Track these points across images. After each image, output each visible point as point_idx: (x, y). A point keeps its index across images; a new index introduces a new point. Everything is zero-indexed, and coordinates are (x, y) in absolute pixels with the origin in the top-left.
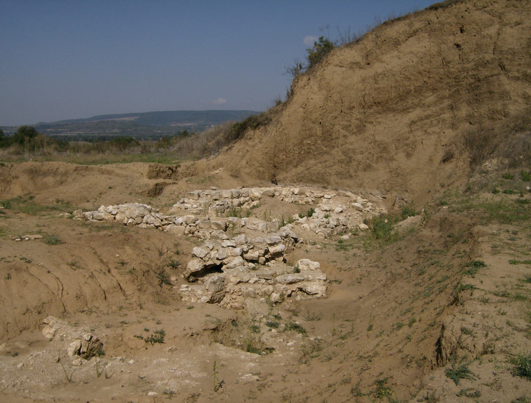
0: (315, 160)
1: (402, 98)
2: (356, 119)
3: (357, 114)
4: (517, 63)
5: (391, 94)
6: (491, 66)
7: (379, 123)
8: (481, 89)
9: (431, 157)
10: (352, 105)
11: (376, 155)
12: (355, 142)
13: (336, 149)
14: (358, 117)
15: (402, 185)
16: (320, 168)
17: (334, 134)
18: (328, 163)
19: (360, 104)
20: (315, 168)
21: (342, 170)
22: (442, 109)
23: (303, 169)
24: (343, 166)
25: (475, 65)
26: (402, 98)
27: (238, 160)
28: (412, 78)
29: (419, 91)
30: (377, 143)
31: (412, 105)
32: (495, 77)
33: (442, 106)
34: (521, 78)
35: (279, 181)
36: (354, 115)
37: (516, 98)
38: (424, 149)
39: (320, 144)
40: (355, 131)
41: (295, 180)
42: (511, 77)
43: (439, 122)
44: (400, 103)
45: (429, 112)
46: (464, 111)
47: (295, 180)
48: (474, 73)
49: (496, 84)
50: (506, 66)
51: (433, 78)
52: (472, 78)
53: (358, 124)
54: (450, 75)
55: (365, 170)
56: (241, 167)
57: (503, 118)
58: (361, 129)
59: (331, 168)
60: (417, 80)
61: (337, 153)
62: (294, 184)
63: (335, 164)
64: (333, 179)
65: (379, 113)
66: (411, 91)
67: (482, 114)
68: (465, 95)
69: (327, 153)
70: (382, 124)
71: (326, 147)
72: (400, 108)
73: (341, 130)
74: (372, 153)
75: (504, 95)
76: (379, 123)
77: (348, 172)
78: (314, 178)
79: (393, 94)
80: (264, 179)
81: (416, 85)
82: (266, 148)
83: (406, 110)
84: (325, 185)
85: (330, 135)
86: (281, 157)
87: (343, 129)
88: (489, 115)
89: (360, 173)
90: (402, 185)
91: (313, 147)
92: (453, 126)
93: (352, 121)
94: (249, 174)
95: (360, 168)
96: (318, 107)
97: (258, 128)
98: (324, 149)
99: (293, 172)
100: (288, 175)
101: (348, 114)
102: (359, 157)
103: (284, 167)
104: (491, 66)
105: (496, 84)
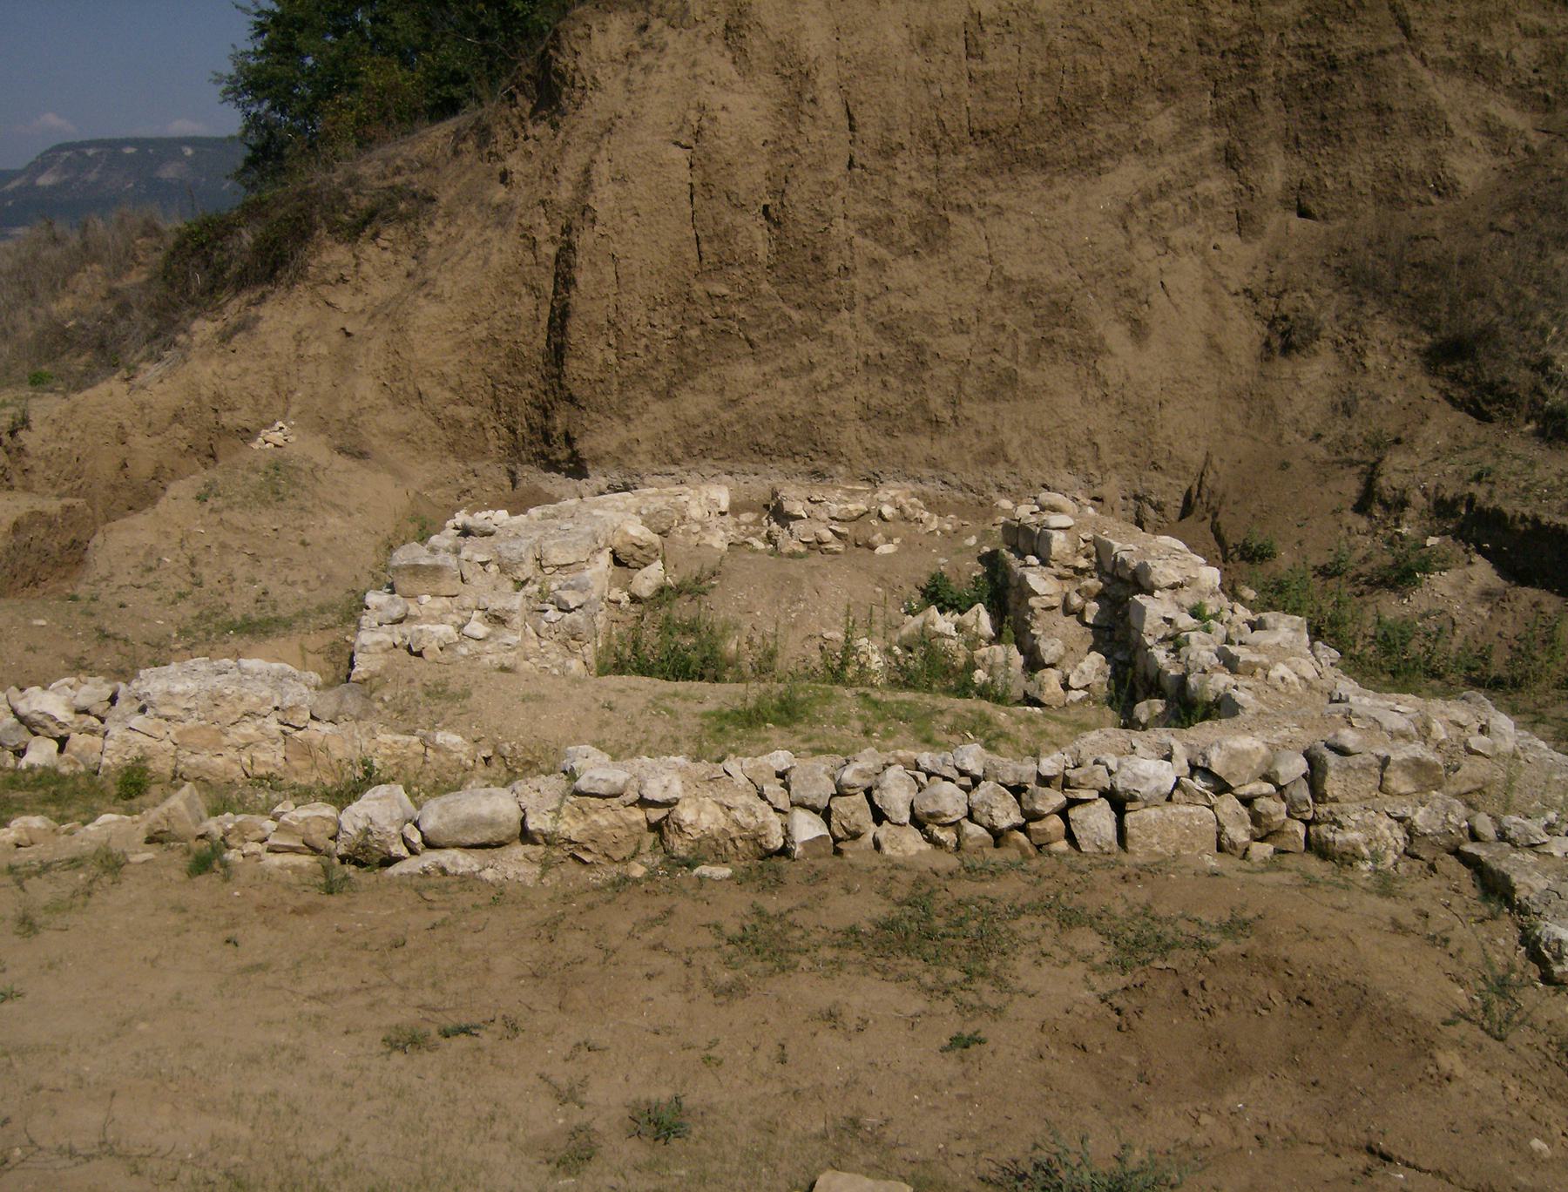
0: (758, 363)
1: (1069, 115)
2: (912, 194)
3: (910, 173)
4: (1441, 15)
5: (1030, 98)
6: (1368, 18)
7: (999, 211)
8: (1343, 97)
9: (1209, 337)
10: (896, 138)
11: (1023, 336)
12: (920, 286)
13: (845, 314)
14: (920, 185)
15: (1137, 444)
16: (788, 396)
17: (832, 254)
18: (820, 375)
19: (926, 134)
20: (763, 395)
21: (892, 398)
22: (1199, 162)
23: (709, 402)
24: (893, 381)
25: (1309, 10)
26: (1069, 115)
27: (325, 386)
28: (1106, 42)
29: (1124, 94)
30: (1020, 289)
31: (1110, 145)
32: (1392, 58)
33: (1197, 151)
34: (1459, 65)
35: (597, 460)
36: (900, 180)
37: (1467, 134)
38: (1176, 306)
39: (771, 298)
40: (910, 240)
41: (678, 453)
42: (1434, 62)
43: (1193, 208)
44: (1064, 137)
45: (1162, 173)
46: (1276, 173)
47: (678, 453)
48: (1305, 40)
49: (1400, 81)
50: (1413, 23)
51: (1165, 47)
52: (1298, 57)
53: (919, 214)
54: (1211, 42)
55: (992, 395)
56: (361, 411)
57: (1435, 200)
58: (932, 235)
59: (835, 394)
60: (1118, 51)
61: (848, 327)
62: (673, 469)
63: (848, 375)
64: (851, 436)
65: (986, 172)
66: (1100, 91)
67: (1356, 183)
68: (1272, 116)
69: (809, 332)
70: (1011, 215)
71: (799, 307)
72: (1068, 153)
73: (858, 240)
74: (1010, 329)
75: (1427, 122)
76: (999, 211)
77: (922, 405)
78: (768, 438)
79: (1037, 100)
80: (483, 453)
81: (1119, 69)
82: (474, 319)
83: (1089, 164)
84: (821, 464)
85: (816, 259)
86: (599, 358)
87: (862, 232)
88: (1378, 185)
89: (969, 409)
90: (1137, 444)
91: (741, 311)
92: (1244, 224)
93: (895, 201)
94: (404, 437)
95: (968, 390)
96: (758, 144)
97: (368, 231)
98: (796, 316)
99: (655, 418)
100: (638, 431)
101: (879, 173)
102: (958, 345)
103: (614, 398)
104: (1368, 18)
105: (1400, 81)
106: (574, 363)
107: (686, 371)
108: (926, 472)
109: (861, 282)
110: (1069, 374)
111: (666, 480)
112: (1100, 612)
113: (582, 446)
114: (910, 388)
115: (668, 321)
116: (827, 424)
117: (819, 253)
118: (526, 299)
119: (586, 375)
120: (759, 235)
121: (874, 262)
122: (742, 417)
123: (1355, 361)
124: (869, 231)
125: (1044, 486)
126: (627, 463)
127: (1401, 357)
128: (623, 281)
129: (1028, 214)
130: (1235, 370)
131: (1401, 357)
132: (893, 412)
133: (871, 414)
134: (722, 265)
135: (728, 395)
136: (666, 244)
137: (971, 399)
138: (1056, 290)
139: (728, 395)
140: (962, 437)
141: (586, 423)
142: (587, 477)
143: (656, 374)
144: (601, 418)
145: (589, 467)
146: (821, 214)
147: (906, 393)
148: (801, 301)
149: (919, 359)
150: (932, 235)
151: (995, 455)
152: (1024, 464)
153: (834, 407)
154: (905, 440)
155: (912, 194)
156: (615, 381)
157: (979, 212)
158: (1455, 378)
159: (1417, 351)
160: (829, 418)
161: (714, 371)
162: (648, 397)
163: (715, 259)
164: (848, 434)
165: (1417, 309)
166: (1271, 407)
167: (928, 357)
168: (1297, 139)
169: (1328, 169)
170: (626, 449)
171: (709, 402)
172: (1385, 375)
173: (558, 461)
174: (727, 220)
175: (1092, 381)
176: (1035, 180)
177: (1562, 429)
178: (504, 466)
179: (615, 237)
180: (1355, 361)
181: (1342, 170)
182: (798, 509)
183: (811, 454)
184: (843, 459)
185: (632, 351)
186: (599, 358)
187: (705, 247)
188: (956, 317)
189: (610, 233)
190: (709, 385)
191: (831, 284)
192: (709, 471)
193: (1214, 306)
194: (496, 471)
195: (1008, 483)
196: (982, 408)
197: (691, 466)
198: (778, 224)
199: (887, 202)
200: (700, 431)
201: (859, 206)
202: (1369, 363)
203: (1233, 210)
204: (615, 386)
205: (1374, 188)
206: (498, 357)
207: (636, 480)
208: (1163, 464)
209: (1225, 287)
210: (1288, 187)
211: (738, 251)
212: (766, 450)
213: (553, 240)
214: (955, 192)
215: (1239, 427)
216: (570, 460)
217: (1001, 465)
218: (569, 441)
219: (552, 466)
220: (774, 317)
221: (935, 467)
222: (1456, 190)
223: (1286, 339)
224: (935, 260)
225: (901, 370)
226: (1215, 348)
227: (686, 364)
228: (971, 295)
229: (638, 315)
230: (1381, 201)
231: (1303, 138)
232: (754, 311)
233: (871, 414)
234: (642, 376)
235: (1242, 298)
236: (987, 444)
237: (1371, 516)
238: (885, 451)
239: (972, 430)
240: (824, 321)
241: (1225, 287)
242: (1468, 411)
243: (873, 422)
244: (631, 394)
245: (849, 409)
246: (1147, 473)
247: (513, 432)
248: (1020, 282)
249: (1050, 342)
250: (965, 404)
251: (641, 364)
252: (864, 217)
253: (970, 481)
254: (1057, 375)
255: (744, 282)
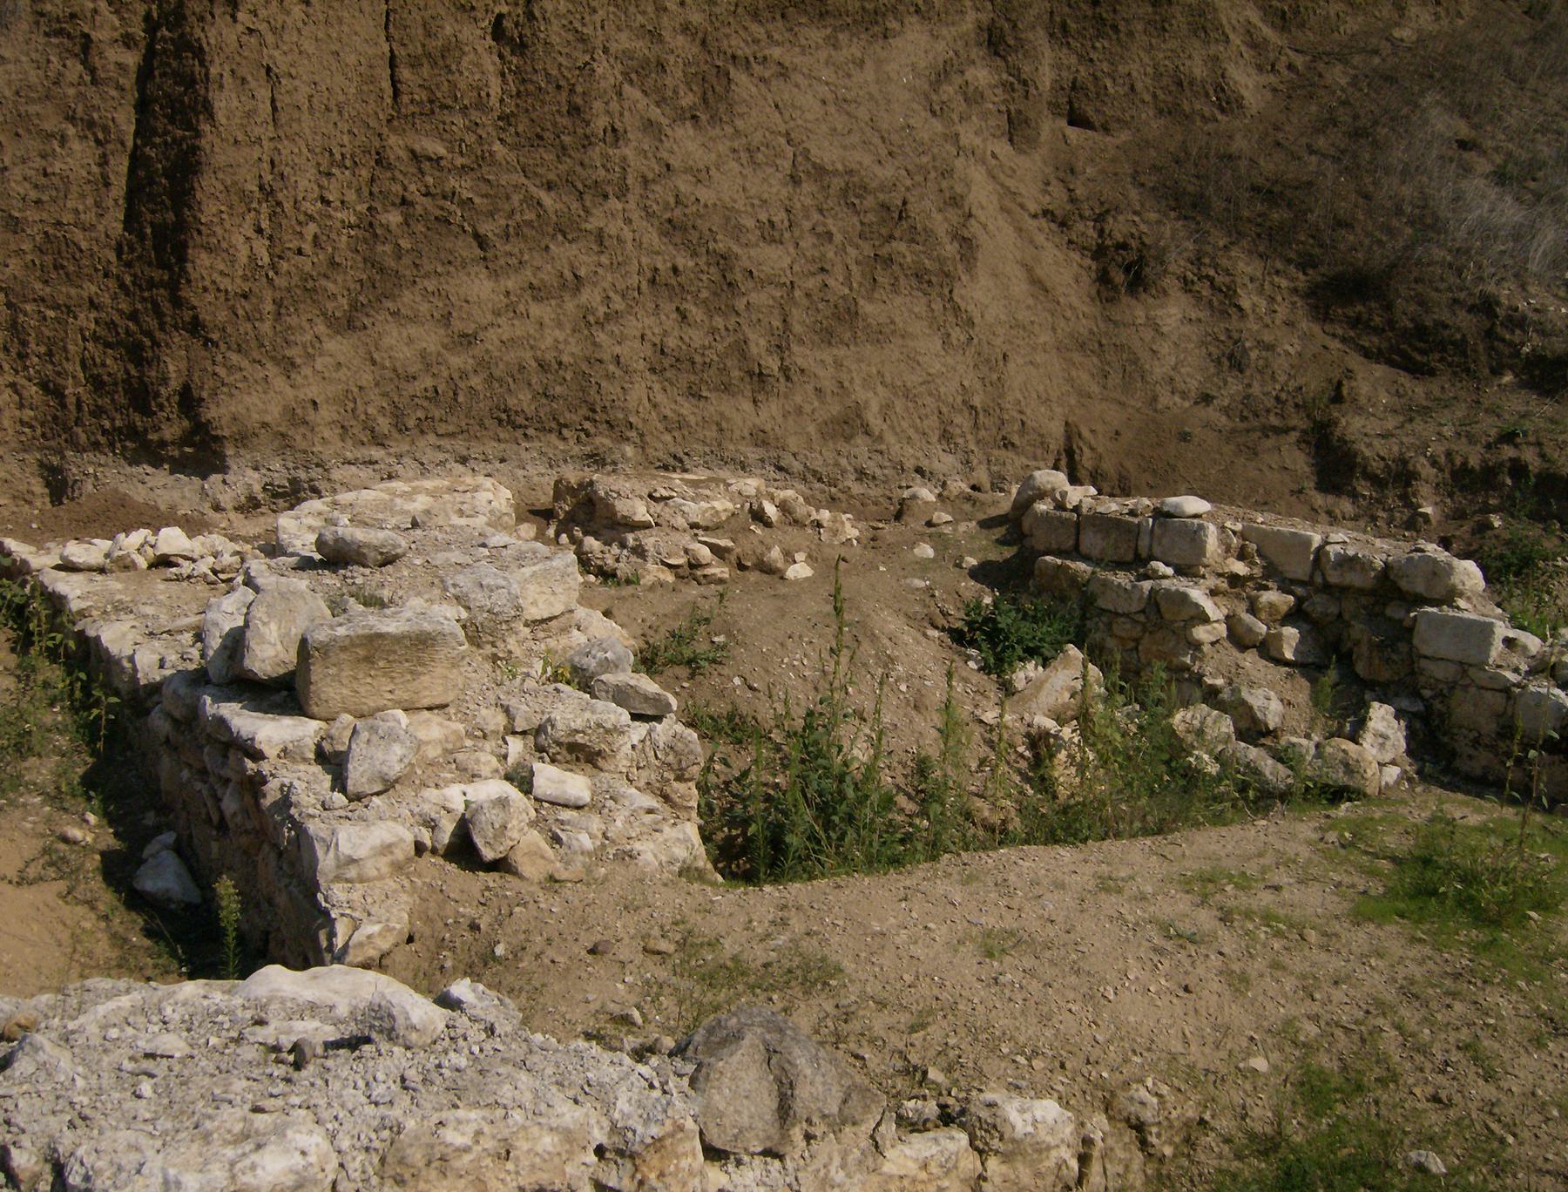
0: (495, 275)
2: (686, 28)
7: (784, 72)
16: (550, 330)
17: (598, 105)
18: (590, 296)
20: (507, 328)
21: (697, 337)
24: (696, 313)
35: (243, 439)
40: (687, 100)
41: (384, 424)
46: (1047, 67)
47: (384, 424)
55: (827, 336)
58: (711, 99)
62: (376, 453)
64: (640, 395)
67: (1139, 86)
69: (565, 230)
71: (550, 186)
74: (838, 238)
77: (741, 349)
78: (522, 400)
85: (574, 110)
86: (243, 255)
91: (464, 186)
98: (547, 199)
103: (266, 327)
106: (204, 259)
107: (383, 281)
108: (752, 454)
109: (633, 153)
110: (920, 308)
111: (365, 473)
112: (1301, 642)
113: (219, 412)
114: (719, 322)
115: (351, 196)
116: (610, 377)
117: (579, 101)
118: (76, 145)
119: (225, 283)
120: (490, 63)
121: (649, 125)
122: (483, 364)
123: (1224, 299)
124: (633, 76)
125: (919, 470)
126: (300, 443)
127: (1279, 298)
128: (283, 118)
129: (819, 80)
130: (1069, 314)
131: (1279, 298)
132: (698, 359)
133: (667, 362)
134: (434, 106)
135: (458, 326)
136: (352, 59)
137: (801, 342)
138: (882, 188)
139: (458, 326)
140: (798, 399)
141: (222, 371)
142: (223, 469)
143: (331, 287)
144: (245, 363)
145: (230, 451)
146: (583, 40)
147: (713, 331)
148: (552, 176)
149: (727, 280)
150: (711, 99)
151: (849, 424)
152: (890, 438)
153: (618, 350)
154: (718, 405)
155: (686, 28)
156: (268, 295)
157: (757, 69)
158: (1355, 322)
159: (1295, 291)
160: (612, 368)
161: (431, 285)
162: (321, 328)
163: (424, 96)
164: (638, 393)
165: (1271, 241)
166: (1135, 361)
167: (739, 276)
168: (1064, 26)
169: (1105, 66)
170: (294, 417)
171: (431, 339)
172: (1268, 320)
173: (163, 444)
174: (448, 30)
175: (951, 319)
176: (815, 35)
177: (1554, 375)
178: (32, 458)
179: (270, 39)
180: (1224, 299)
181: (1122, 69)
182: (641, 512)
183: (587, 425)
184: (633, 434)
185: (293, 245)
186: (243, 255)
187: (405, 73)
188: (763, 217)
189: (263, 27)
190: (424, 308)
191: (595, 154)
192: (430, 456)
193: (1019, 230)
194: (14, 467)
195: (871, 467)
196: (819, 355)
197: (405, 447)
198: (521, 47)
199: (655, 36)
200: (418, 387)
201: (623, 36)
202: (1246, 304)
203: (1003, 108)
204: (268, 307)
205: (1155, 96)
206: (20, 253)
207: (316, 473)
208: (1016, 439)
209: (1022, 206)
210: (1057, 87)
211: (462, 85)
212: (520, 420)
213: (128, 41)
214: (727, 36)
215: (1095, 389)
216: (185, 440)
217: (860, 439)
218: (188, 401)
219: (148, 453)
220: (516, 198)
221: (765, 443)
222: (1241, 106)
223: (1122, 272)
224: (718, 131)
225: (704, 294)
226: (1039, 286)
227: (381, 270)
228: (776, 188)
229: (305, 182)
230: (1161, 112)
231: (1073, 26)
232: (485, 188)
233: (667, 362)
234: (309, 289)
235: (1043, 222)
236: (835, 409)
237: (1354, 496)
238: (692, 420)
239: (810, 388)
240: (587, 211)
241: (1022, 206)
242: (1391, 363)
243: (668, 374)
244: (293, 320)
245: (635, 353)
246: (996, 452)
247: (58, 393)
248: (835, 173)
249: (889, 261)
250: (795, 348)
251: (308, 268)
252: (628, 54)
253: (817, 464)
254: (899, 308)
255: (471, 138)
